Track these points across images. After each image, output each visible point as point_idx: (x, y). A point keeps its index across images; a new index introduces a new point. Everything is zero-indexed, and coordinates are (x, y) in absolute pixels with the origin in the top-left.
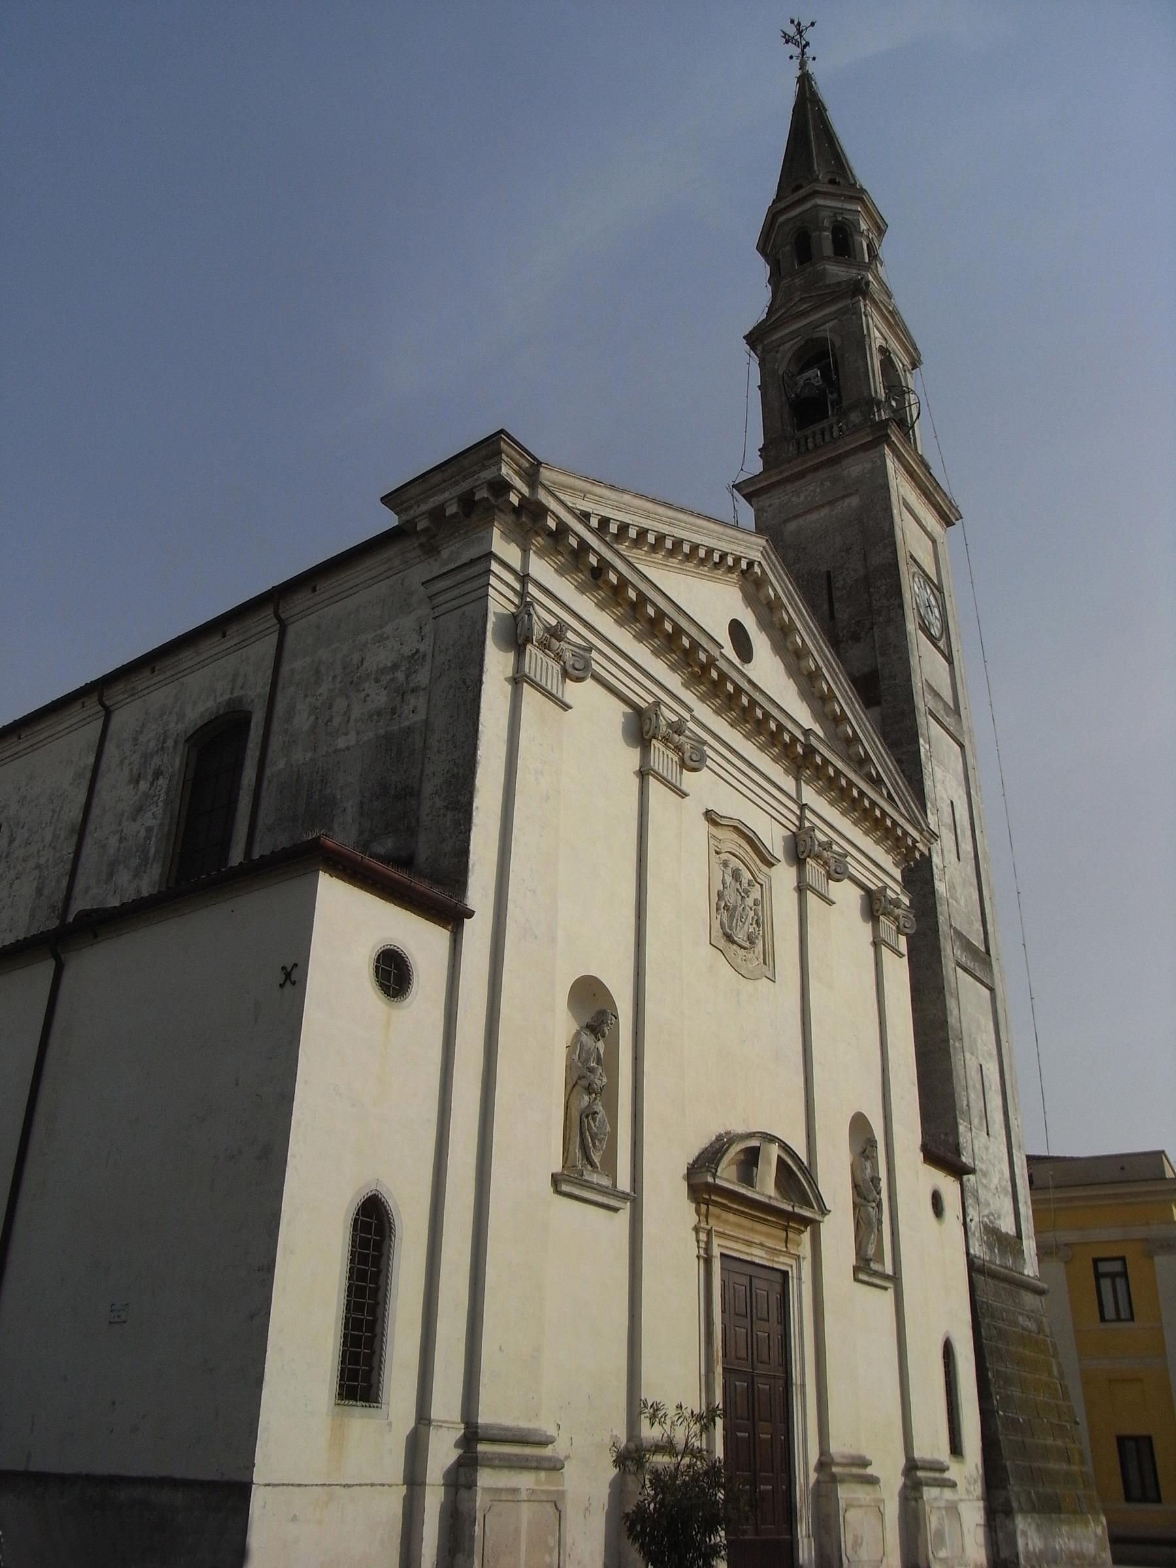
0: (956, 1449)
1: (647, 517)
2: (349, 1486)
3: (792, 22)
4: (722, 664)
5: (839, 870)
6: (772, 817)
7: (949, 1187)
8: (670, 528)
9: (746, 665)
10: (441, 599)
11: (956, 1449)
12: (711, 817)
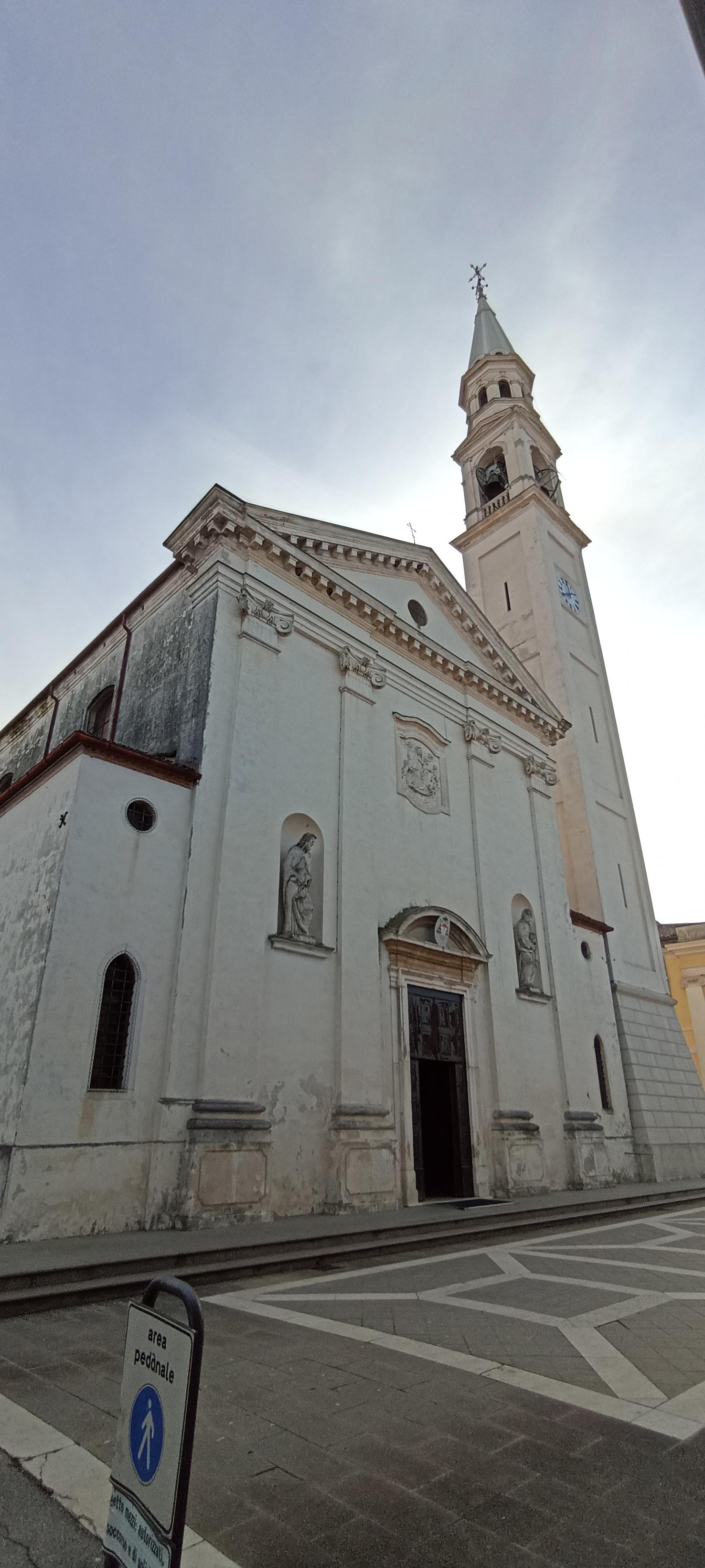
0: (606, 1104)
1: (335, 537)
2: (97, 1145)
3: (472, 266)
4: (408, 630)
5: (495, 746)
6: (445, 716)
7: (594, 939)
8: (353, 544)
9: (422, 627)
10: (196, 595)
11: (606, 1104)
12: (398, 717)
